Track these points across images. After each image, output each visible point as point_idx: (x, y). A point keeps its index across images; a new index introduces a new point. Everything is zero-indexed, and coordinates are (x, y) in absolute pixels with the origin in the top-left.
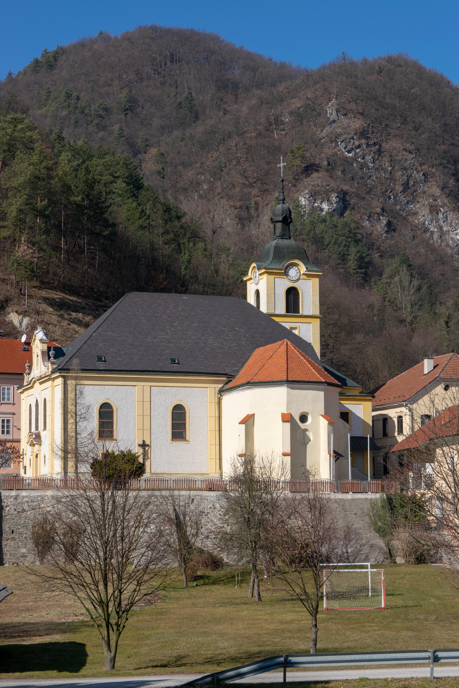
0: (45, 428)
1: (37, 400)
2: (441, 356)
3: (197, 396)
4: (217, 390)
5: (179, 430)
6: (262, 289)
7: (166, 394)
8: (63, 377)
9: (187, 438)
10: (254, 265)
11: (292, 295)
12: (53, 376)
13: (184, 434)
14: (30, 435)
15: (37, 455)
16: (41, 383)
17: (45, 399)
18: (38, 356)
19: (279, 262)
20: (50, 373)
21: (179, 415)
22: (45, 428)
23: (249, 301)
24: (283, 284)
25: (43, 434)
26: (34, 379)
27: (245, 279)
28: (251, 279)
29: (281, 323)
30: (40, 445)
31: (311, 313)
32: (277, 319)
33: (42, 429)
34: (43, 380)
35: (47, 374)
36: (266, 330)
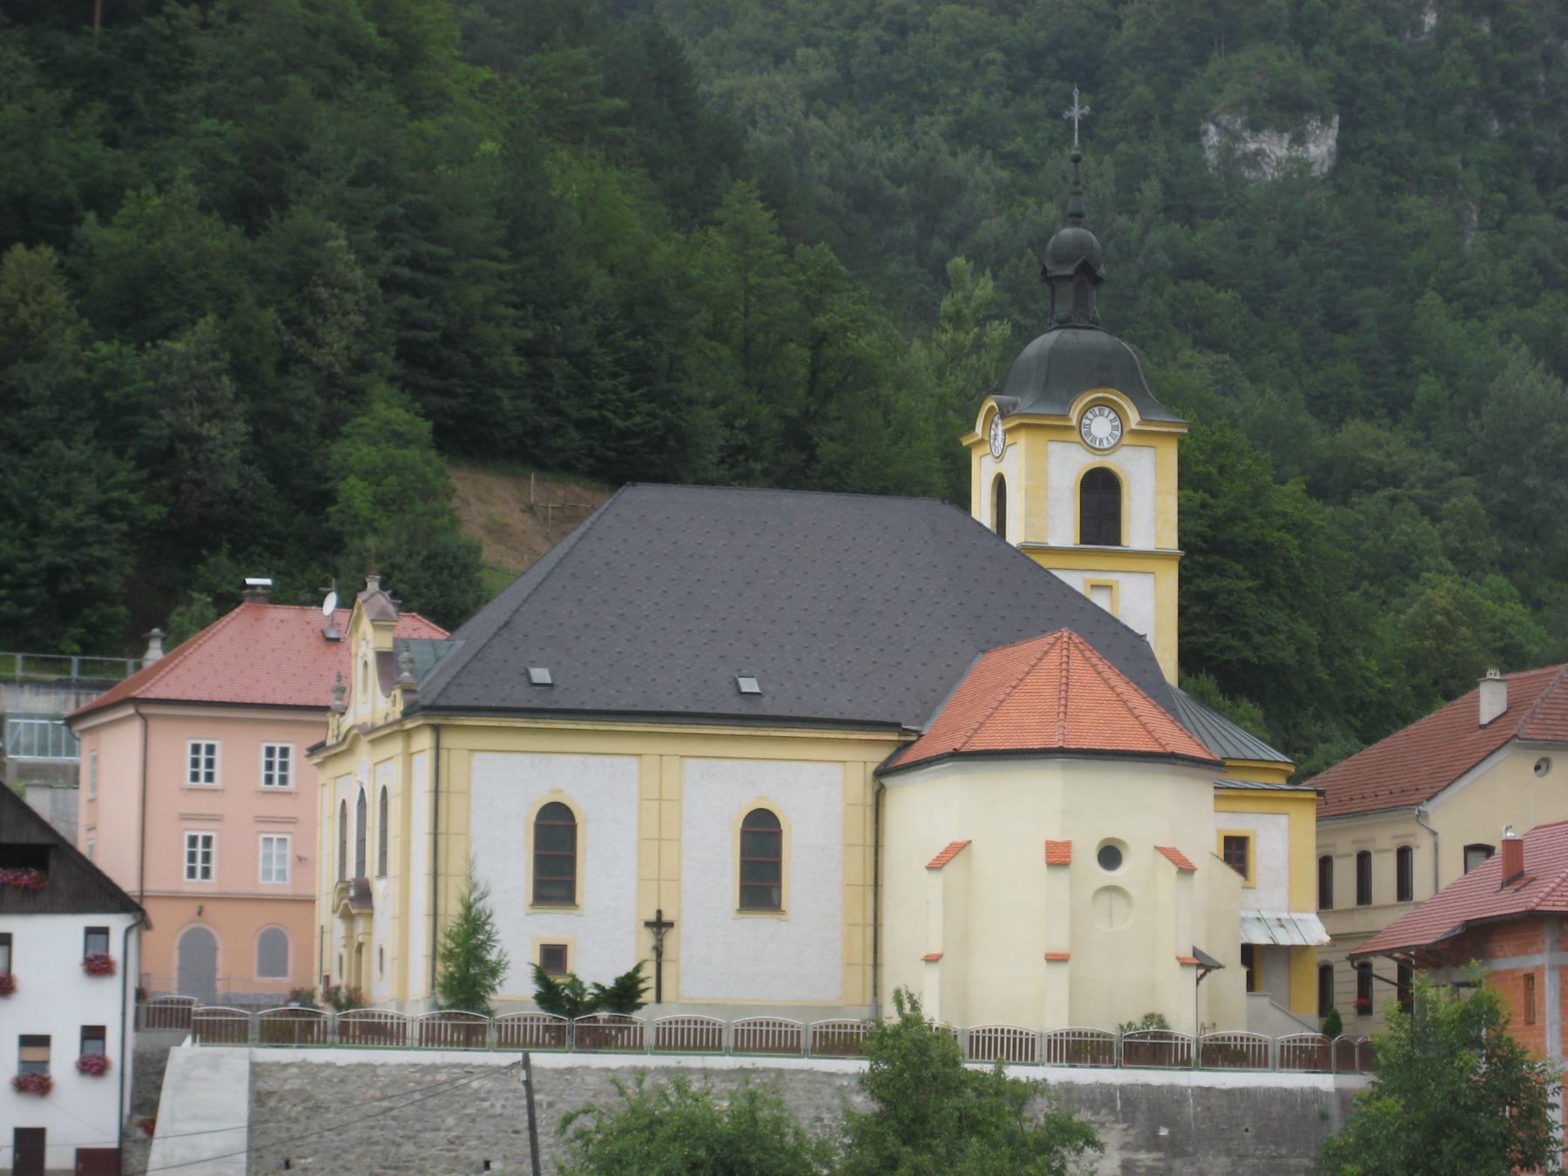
0: (383, 872)
1: (362, 791)
2: (1533, 673)
3: (812, 787)
4: (872, 767)
5: (761, 881)
6: (1025, 479)
7: (718, 783)
8: (437, 729)
9: (784, 906)
10: (991, 402)
11: (1101, 498)
12: (409, 725)
13: (775, 895)
14: (342, 890)
15: (360, 946)
16: (373, 742)
17: (384, 790)
18: (366, 664)
19: (1054, 392)
20: (398, 716)
21: (761, 840)
22: (383, 872)
23: (975, 514)
24: (1067, 466)
25: (379, 888)
26: (355, 731)
27: (966, 442)
28: (981, 442)
29: (1055, 573)
30: (371, 915)
31: (1148, 546)
32: (1044, 561)
33: (376, 872)
34: (376, 734)
35: (390, 719)
36: (1023, 597)
